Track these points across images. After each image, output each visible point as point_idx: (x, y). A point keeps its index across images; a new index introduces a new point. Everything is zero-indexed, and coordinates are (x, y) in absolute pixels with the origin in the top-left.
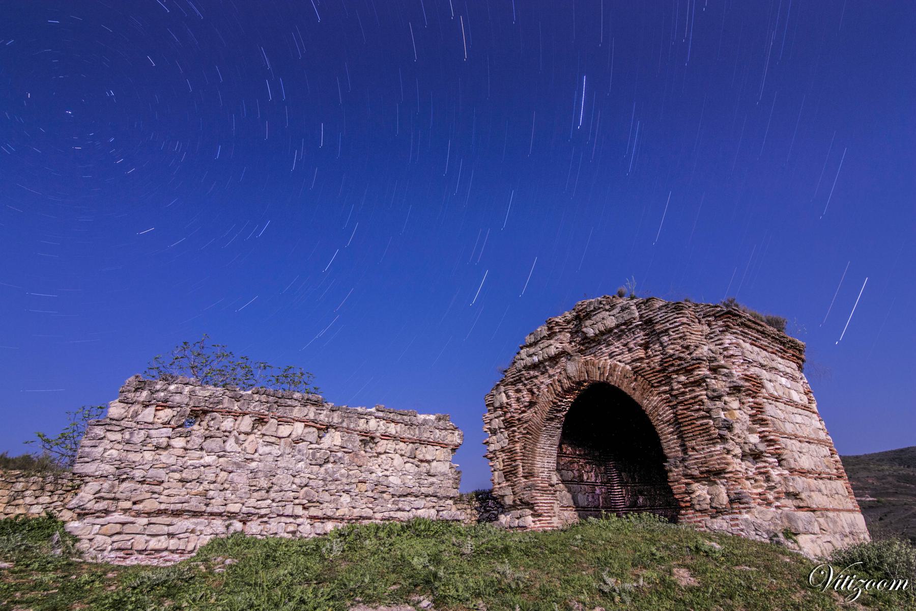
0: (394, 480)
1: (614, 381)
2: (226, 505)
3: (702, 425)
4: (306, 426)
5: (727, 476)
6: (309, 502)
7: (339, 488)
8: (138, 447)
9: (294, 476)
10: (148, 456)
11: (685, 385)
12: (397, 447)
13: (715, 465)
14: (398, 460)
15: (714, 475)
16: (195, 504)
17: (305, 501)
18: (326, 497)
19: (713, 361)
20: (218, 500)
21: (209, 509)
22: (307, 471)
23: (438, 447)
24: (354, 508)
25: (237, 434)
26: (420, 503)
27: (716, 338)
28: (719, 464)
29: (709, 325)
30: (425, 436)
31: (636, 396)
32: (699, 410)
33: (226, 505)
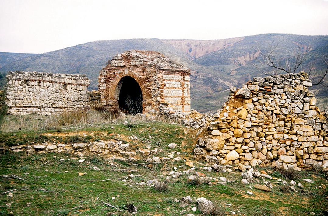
0: (72, 97)
4: (50, 83)
8: (17, 91)
10: (19, 93)
11: (148, 85)
14: (73, 91)
16: (30, 105)
17: (52, 103)
18: (56, 102)
20: (34, 104)
21: (33, 106)
26: (79, 103)
30: (79, 83)
31: (139, 84)
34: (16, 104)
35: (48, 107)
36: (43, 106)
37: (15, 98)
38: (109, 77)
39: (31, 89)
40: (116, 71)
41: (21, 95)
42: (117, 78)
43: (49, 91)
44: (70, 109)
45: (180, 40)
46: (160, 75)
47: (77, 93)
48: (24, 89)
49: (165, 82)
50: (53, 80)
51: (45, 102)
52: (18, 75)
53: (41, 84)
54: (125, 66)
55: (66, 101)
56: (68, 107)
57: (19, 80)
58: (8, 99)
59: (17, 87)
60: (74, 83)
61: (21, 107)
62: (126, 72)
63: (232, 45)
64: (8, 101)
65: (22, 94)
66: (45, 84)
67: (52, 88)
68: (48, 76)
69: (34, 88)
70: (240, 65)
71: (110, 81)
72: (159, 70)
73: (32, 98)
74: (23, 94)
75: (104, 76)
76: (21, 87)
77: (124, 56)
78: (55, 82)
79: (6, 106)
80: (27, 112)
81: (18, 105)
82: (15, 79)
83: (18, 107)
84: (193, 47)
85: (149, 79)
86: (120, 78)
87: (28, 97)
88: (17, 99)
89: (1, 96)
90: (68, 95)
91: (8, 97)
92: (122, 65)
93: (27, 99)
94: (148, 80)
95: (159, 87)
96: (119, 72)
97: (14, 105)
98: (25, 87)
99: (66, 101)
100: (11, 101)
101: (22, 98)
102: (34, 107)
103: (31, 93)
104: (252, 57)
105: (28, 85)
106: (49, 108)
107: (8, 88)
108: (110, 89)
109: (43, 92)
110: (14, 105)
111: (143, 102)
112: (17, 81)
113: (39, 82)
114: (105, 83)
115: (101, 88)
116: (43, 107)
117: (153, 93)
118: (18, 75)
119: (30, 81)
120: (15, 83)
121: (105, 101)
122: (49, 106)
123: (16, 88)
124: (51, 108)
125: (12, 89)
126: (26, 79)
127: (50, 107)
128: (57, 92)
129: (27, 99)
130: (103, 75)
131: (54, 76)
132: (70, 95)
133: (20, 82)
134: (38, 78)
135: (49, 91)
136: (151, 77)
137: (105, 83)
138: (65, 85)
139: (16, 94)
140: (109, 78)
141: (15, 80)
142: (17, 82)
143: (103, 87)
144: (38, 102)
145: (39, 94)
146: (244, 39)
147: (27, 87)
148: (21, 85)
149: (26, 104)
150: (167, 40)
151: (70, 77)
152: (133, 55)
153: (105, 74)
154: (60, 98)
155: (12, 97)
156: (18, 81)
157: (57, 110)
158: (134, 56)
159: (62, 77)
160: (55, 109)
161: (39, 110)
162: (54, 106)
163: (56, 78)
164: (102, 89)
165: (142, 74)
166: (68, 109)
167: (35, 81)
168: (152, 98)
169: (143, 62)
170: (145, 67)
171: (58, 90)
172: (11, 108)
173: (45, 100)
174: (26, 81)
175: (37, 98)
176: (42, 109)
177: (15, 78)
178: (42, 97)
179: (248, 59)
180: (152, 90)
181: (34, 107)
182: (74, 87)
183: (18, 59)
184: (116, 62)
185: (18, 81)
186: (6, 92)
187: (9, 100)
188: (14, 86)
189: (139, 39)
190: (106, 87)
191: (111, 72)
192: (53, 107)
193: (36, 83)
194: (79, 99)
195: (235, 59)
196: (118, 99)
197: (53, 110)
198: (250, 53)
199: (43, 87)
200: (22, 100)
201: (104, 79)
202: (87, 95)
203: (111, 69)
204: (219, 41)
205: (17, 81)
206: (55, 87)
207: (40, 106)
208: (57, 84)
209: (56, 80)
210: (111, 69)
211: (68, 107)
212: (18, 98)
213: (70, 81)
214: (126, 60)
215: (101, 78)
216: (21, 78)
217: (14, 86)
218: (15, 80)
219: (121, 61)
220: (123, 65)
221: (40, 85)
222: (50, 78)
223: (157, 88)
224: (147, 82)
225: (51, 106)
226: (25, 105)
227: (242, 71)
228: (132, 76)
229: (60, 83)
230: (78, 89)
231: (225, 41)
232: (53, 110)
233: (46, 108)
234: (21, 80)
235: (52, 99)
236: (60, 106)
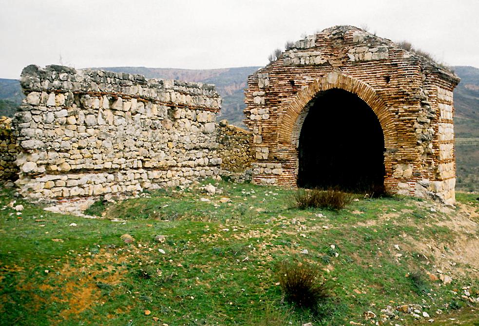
0: (187, 139)
1: (362, 96)
2: (103, 163)
3: (409, 135)
4: (138, 101)
5: (414, 162)
6: (145, 157)
7: (160, 146)
8: (51, 126)
9: (135, 140)
10: (59, 131)
11: (406, 111)
12: (187, 113)
13: (411, 156)
14: (188, 124)
15: (408, 161)
16: (88, 165)
17: (142, 158)
18: (153, 154)
19: (423, 100)
20: (100, 161)
21: (96, 167)
22: (141, 136)
23: (209, 112)
24: (167, 160)
25: (102, 111)
26: (200, 154)
27: (428, 85)
28: (413, 157)
29: (426, 75)
30: (202, 103)
31: (375, 109)
32: (410, 127)
33: (103, 163)
34: (48, 164)
35: (133, 168)
36: (123, 166)
37: (45, 147)
38: (276, 90)
39: (90, 119)
40: (297, 75)
41: (63, 137)
42: (303, 94)
43: (137, 126)
44: (184, 169)
45: (167, 69)
46: (433, 86)
47: (198, 129)
48: (72, 120)
49: (441, 106)
50: (145, 94)
51: (126, 155)
52: (57, 78)
53: (118, 105)
54: (327, 63)
55: (175, 150)
56: (180, 165)
57: (59, 91)
58: (26, 151)
59: (52, 114)
60: (192, 104)
61: (63, 173)
62: (332, 79)
63: (218, 75)
64: (26, 157)
65: (67, 132)
66: (127, 106)
67: (143, 117)
68: (135, 85)
69: (100, 116)
70: (227, 94)
71: (280, 102)
72: (433, 74)
73: (94, 144)
74: (70, 134)
75: (264, 89)
76: (65, 112)
77: (326, 40)
78: (151, 100)
79: (18, 168)
80: (79, 186)
81: (54, 168)
82: (46, 87)
83: (56, 172)
84: (179, 75)
85: (408, 95)
86: (313, 94)
87: (83, 143)
88: (53, 150)
89: (3, 138)
90: (178, 134)
91: (25, 144)
92: (318, 61)
93: (80, 148)
94: (402, 97)
95: (431, 118)
96: (308, 79)
97: (42, 169)
98: (75, 114)
99: (175, 150)
100: (35, 156)
101: (67, 145)
102: (98, 170)
103: (91, 131)
104: (238, 87)
105: (82, 107)
106: (135, 171)
107: (28, 115)
108: (279, 121)
109: (122, 128)
110: (42, 169)
111: (388, 157)
112: (52, 95)
113: (113, 100)
114: (266, 105)
115: (252, 117)
116: (120, 169)
117: (419, 131)
118: (57, 78)
119: (88, 96)
120: (46, 100)
121: (266, 150)
122: (135, 166)
123: (51, 117)
124: (142, 171)
125: (38, 119)
126: (78, 88)
127: (138, 168)
128: (155, 128)
129: (80, 148)
130: (261, 86)
131: (149, 84)
132: (183, 134)
133: (62, 98)
134: (109, 89)
135: (137, 126)
136: (414, 89)
137: (266, 105)
138: (173, 108)
139: (50, 133)
140: (276, 94)
141: (49, 93)
142: (52, 99)
143: (260, 114)
144: (110, 155)
145: (112, 133)
146: (230, 71)
147: (82, 112)
148: (65, 107)
149: (78, 162)
150: (154, 69)
151: (184, 89)
152: (358, 37)
153: (267, 83)
154: (162, 141)
155: (39, 144)
156: (57, 93)
157: (155, 174)
158: (361, 39)
159: (167, 87)
160: (149, 172)
161: (111, 177)
162: (147, 165)
163: (153, 91)
164: (255, 121)
165: (382, 82)
166: (177, 171)
167: (103, 95)
168: (418, 144)
169: (390, 52)
170: (396, 65)
171: (158, 122)
172: (32, 176)
173: (127, 149)
174: (79, 95)
175: (108, 144)
176: (119, 174)
177: (46, 84)
178: (119, 141)
179: (234, 89)
180: (416, 125)
181: (98, 170)
182: (191, 114)
183: (6, 84)
184: (300, 54)
185: (57, 93)
186: (20, 129)
187: (29, 154)
188: (44, 109)
189: (127, 67)
190: (268, 116)
191: (281, 79)
192: (144, 168)
193: (106, 100)
194: (202, 145)
195: (222, 88)
196: (297, 147)
197: (144, 176)
198: (236, 83)
199: (122, 113)
200: (67, 151)
201: (262, 96)
202: (215, 133)
203: (285, 72)
204: (205, 71)
205: (52, 95)
206: (149, 114)
207: (114, 166)
208: (155, 106)
209: (153, 94)
210: (285, 72)
211: (180, 165)
212: (56, 145)
213: (184, 99)
214: (328, 50)
215: (255, 93)
216: (65, 84)
217: (44, 109)
218: (49, 93)
219: (315, 53)
220: (322, 62)
221: (114, 107)
222: (139, 90)
223: (429, 121)
224: (403, 102)
225: (140, 165)
226: (73, 167)
227: (230, 100)
228: (349, 89)
229: (161, 103)
230: (199, 120)
231: (211, 71)
232: (144, 176)
233: (129, 172)
234: (63, 93)
235: (142, 146)
236: (161, 164)
